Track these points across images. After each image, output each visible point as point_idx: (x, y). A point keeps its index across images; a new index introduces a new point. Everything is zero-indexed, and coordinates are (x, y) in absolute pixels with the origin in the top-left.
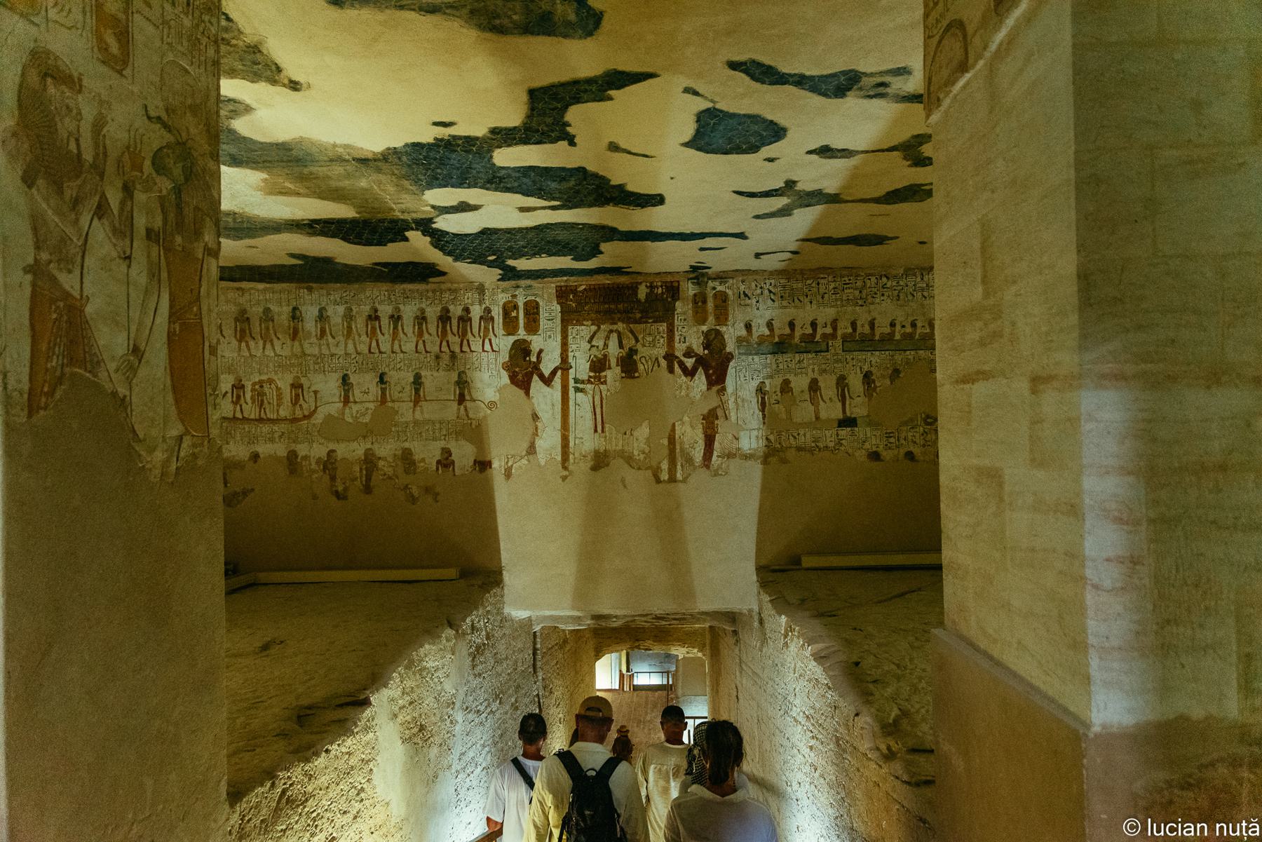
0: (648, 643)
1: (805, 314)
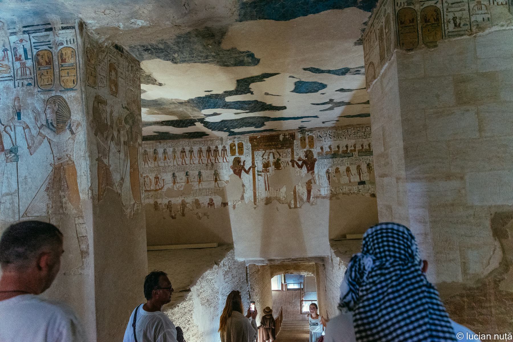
0: (292, 271)
1: (343, 142)
